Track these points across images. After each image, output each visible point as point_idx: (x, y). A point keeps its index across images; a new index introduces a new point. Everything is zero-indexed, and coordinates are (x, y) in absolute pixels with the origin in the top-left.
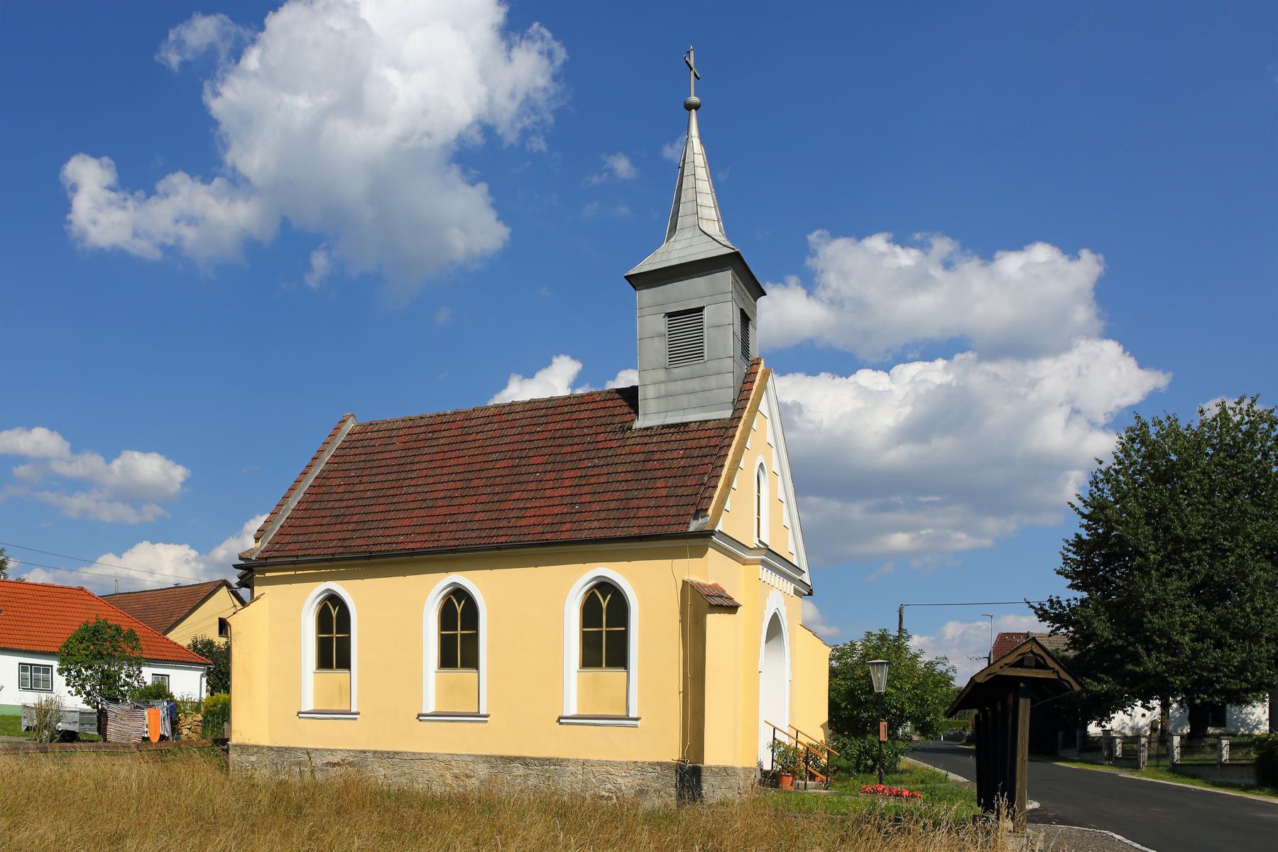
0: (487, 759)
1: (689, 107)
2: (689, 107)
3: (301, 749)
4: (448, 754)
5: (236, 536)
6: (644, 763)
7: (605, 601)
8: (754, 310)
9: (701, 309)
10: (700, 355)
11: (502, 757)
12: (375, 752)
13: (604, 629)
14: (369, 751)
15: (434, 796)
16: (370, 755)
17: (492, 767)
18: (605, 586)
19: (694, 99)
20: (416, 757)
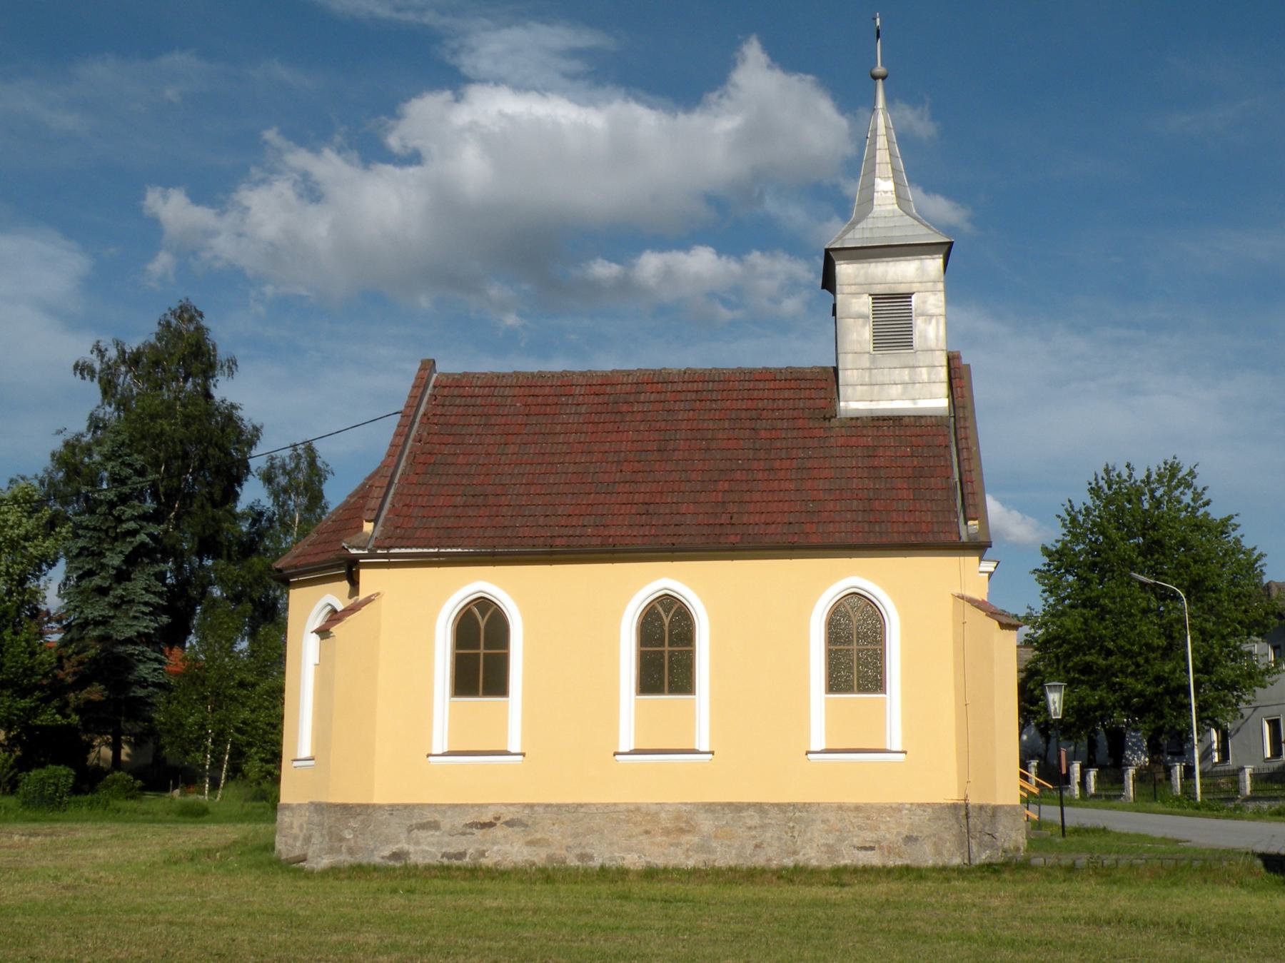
0: (710, 808)
1: (875, 78)
2: (875, 78)
3: (429, 805)
4: (657, 804)
5: (58, 455)
6: (912, 804)
7: (483, 618)
8: (471, 376)
9: (908, 296)
10: (908, 344)
11: (730, 805)
12: (548, 806)
13: (482, 651)
14: (539, 805)
15: (480, 866)
16: (541, 810)
17: (717, 818)
18: (483, 603)
19: (880, 69)
20: (421, 806)
